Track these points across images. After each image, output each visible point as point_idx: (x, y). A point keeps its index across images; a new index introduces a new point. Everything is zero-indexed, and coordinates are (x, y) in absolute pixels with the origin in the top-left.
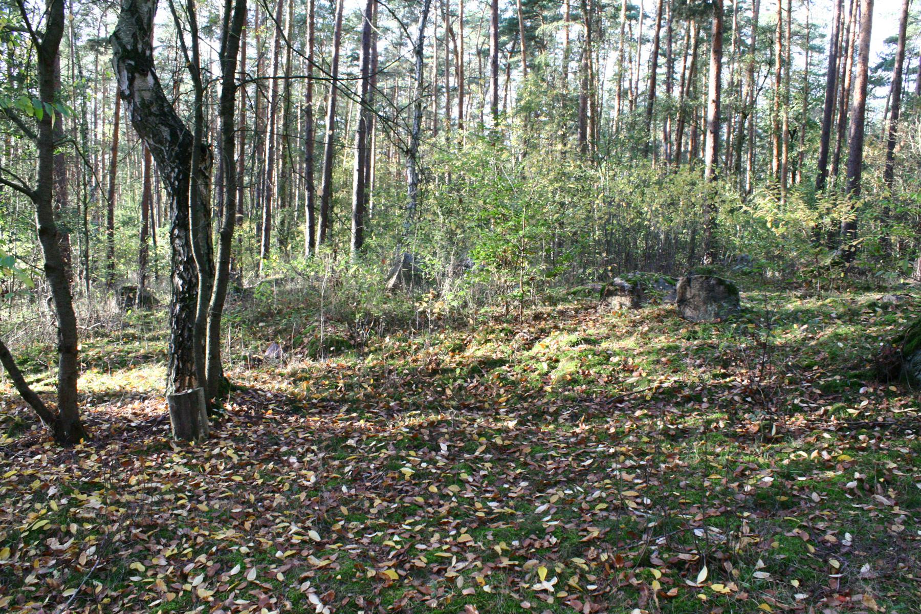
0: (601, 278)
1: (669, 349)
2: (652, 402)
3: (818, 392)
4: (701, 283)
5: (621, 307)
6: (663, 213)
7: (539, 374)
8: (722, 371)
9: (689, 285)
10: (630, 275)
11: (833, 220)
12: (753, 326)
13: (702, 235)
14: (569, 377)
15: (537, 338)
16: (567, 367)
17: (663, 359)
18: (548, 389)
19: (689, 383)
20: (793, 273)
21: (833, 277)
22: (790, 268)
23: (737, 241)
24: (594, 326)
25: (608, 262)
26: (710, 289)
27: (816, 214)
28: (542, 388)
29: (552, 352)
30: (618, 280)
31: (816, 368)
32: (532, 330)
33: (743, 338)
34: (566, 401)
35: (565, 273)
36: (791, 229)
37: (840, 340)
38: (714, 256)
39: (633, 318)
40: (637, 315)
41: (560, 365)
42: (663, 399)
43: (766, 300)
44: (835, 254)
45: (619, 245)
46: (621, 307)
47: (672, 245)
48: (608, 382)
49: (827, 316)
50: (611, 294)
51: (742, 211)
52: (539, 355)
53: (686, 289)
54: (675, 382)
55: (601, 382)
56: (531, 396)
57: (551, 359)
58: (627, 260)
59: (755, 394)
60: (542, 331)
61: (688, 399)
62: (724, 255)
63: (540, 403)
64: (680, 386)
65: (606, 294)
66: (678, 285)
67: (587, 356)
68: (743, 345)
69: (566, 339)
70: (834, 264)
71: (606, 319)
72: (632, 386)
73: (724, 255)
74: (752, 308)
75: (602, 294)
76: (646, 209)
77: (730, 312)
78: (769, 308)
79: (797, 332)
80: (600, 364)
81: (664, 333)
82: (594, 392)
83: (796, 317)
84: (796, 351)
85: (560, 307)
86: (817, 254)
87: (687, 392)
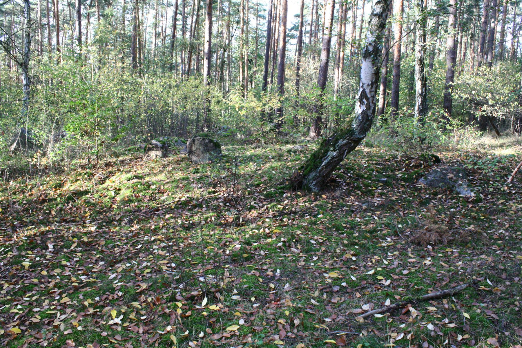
0: (145, 141)
1: (184, 179)
3: (263, 198)
4: (201, 142)
5: (156, 157)
7: (109, 198)
8: (213, 190)
9: (194, 143)
10: (161, 139)
14: (127, 199)
15: (107, 177)
16: (125, 193)
17: (181, 185)
18: (115, 206)
19: (195, 197)
23: (222, 119)
26: (206, 145)
28: (111, 206)
29: (117, 185)
30: (154, 142)
31: (262, 185)
32: (104, 172)
34: (126, 212)
37: (273, 170)
38: (208, 127)
39: (163, 163)
40: (165, 161)
42: (181, 207)
46: (156, 157)
47: (186, 121)
49: (267, 157)
50: (150, 149)
52: (109, 187)
54: (188, 197)
55: (146, 200)
56: (105, 211)
57: (116, 189)
60: (110, 173)
61: (195, 206)
64: (190, 200)
65: (147, 150)
66: (188, 143)
67: (137, 186)
68: (224, 175)
69: (124, 177)
70: (271, 130)
72: (164, 201)
74: (229, 154)
75: (145, 150)
80: (145, 190)
81: (181, 170)
82: (142, 206)
83: (251, 159)
84: (251, 177)
85: (121, 158)
87: (194, 202)
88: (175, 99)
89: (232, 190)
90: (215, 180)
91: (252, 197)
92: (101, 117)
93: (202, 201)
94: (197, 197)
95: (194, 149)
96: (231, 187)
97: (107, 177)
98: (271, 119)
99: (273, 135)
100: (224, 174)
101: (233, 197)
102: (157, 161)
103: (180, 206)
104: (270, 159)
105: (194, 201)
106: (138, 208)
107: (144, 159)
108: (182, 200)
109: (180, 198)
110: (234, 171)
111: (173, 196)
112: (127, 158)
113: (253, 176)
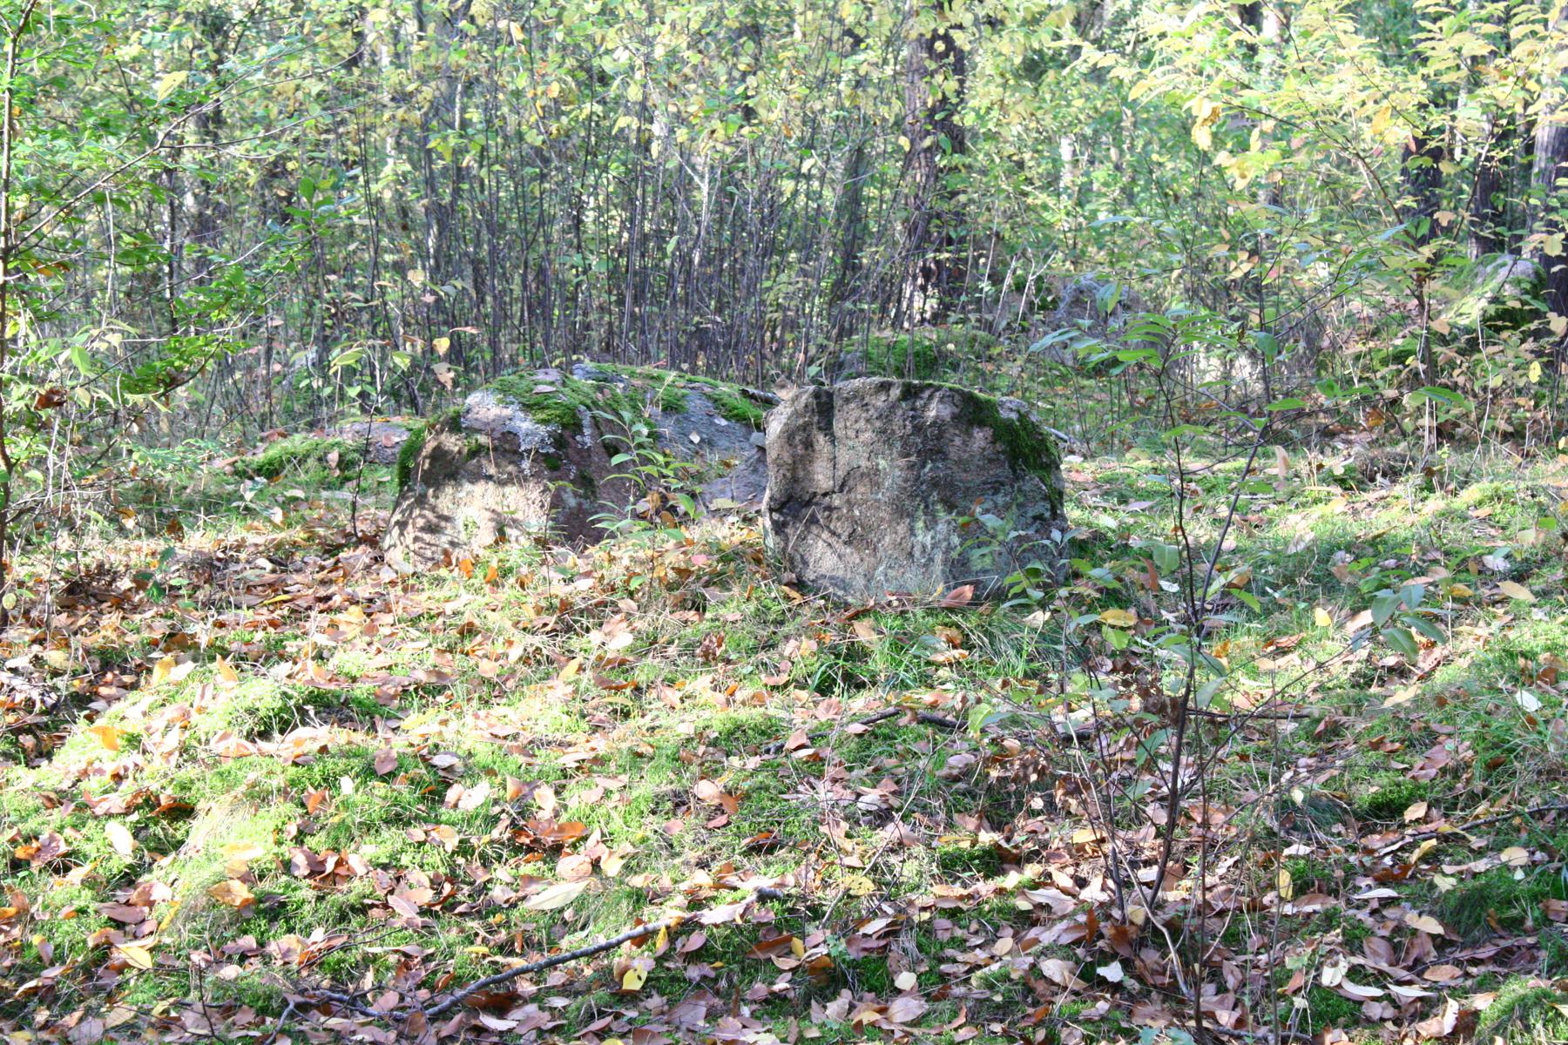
0: (409, 392)
1: (734, 739)
2: (656, 1002)
3: (1431, 926)
4: (886, 416)
5: (502, 537)
6: (704, 76)
7: (90, 883)
8: (987, 838)
9: (827, 428)
10: (546, 381)
11: (1495, 113)
12: (1129, 617)
13: (891, 194)
14: (241, 893)
15: (81, 700)
16: (234, 840)
17: (708, 790)
18: (135, 953)
19: (829, 899)
20: (1317, 359)
21: (1495, 382)
22: (1303, 340)
23: (1059, 214)
24: (371, 630)
25: (442, 316)
26: (927, 446)
27: (1417, 89)
28: (103, 951)
29: (158, 775)
30: (485, 406)
31: (1416, 811)
32: (55, 657)
33: (1078, 681)
34: (228, 1011)
35: (226, 368)
36: (1301, 159)
37: (1523, 678)
38: (949, 281)
39: (560, 590)
40: (575, 575)
41: (197, 832)
42: (706, 985)
43: (1179, 494)
44: (1503, 279)
45: (496, 229)
46: (502, 537)
47: (754, 228)
48: (439, 909)
49: (1468, 566)
50: (446, 470)
51: (1081, 66)
52: (92, 785)
53: (809, 445)
54: (763, 897)
55: (405, 908)
56: (47, 995)
57: (150, 802)
58: (538, 307)
59: (1141, 943)
60: (109, 660)
61: (826, 980)
62: (996, 279)
63: (94, 1028)
64: (796, 915)
65: (427, 473)
66: (776, 426)
67: (330, 781)
68: (1083, 714)
69: (225, 698)
70: (1502, 319)
71: (422, 601)
72: (558, 922)
73: (996, 279)
74: (1125, 531)
75: (405, 475)
76: (623, 56)
77: (1017, 555)
78: (1200, 531)
79: (1326, 650)
80: (398, 820)
81: (709, 657)
82: (369, 960)
83: (1315, 575)
84: (1326, 736)
85: (199, 540)
86: (1423, 276)
87: (818, 944)
88: (665, 40)
89: (1147, 839)
90: (1001, 757)
91: (1329, 920)
92: (39, 188)
93: (891, 932)
94: (849, 896)
95: (822, 477)
96: (1138, 819)
97: (81, 700)
98: (1498, 218)
99: (1511, 365)
100: (1084, 700)
101: (1156, 905)
102: (506, 572)
103: (694, 972)
104: (1487, 575)
105: (816, 933)
106: (339, 975)
107: (395, 556)
108: (717, 914)
109: (696, 903)
110: (1170, 683)
111: (638, 881)
112: (253, 535)
113: (1335, 730)
